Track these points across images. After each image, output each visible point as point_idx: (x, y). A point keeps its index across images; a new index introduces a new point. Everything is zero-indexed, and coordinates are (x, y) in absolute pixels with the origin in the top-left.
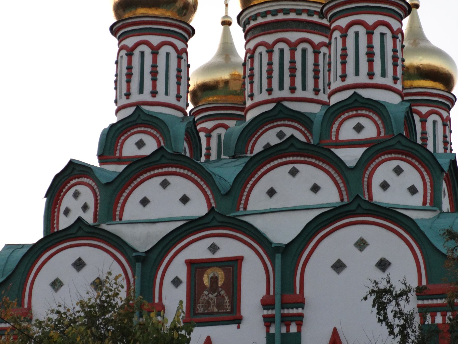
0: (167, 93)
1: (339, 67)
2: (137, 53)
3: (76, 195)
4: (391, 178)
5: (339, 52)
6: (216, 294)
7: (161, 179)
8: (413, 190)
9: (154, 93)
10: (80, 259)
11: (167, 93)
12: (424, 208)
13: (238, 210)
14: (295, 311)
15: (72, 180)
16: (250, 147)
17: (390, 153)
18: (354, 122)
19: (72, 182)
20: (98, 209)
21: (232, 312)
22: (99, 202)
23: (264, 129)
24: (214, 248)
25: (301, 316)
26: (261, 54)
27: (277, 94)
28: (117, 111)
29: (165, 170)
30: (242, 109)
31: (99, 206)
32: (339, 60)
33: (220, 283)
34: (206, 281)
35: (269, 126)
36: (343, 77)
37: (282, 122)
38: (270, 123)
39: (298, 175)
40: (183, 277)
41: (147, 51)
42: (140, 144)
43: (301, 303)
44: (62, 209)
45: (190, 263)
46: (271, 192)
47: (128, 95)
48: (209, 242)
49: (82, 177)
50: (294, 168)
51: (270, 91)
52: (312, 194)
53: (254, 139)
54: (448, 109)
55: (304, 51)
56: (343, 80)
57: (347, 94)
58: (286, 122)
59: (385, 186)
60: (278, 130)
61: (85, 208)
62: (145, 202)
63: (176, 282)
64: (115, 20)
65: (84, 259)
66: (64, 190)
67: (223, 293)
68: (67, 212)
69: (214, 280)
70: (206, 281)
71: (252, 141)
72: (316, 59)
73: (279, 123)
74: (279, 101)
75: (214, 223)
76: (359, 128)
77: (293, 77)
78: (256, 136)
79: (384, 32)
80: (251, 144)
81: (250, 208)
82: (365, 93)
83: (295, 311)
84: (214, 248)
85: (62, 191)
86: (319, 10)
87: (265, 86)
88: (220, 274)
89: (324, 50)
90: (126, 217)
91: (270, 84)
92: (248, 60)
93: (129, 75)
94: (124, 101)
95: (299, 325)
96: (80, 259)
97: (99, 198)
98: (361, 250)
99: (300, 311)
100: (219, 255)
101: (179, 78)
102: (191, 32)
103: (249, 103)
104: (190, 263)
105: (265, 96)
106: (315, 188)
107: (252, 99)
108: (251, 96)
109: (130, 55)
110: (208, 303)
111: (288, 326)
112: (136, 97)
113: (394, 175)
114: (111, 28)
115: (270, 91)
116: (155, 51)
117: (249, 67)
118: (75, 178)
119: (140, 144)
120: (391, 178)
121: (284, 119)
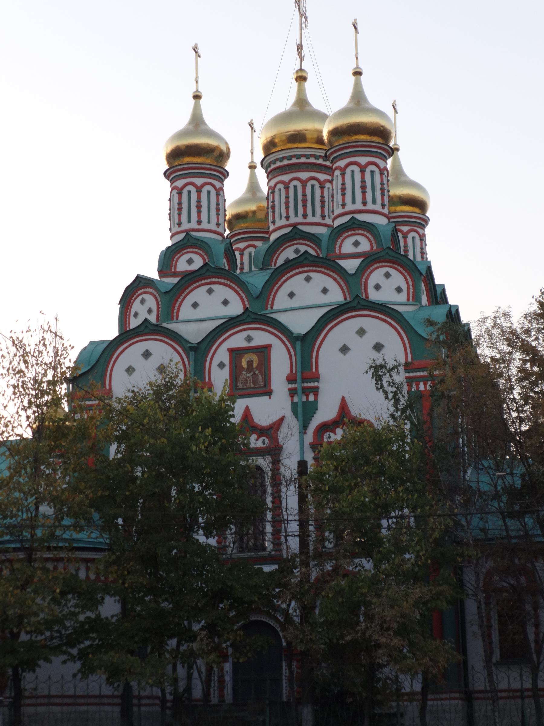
0: (209, 222)
2: (185, 192)
3: (143, 302)
4: (382, 281)
5: (340, 186)
8: (399, 290)
9: (199, 222)
10: (147, 350)
11: (209, 222)
12: (408, 303)
13: (267, 309)
15: (139, 290)
16: (274, 261)
19: (139, 292)
21: (264, 387)
23: (284, 247)
24: (249, 339)
25: (317, 388)
28: (172, 237)
29: (210, 280)
30: (267, 233)
32: (340, 192)
33: (255, 365)
34: (244, 364)
36: (344, 205)
37: (298, 241)
38: (289, 243)
39: (311, 281)
41: (357, 169)
42: (190, 261)
44: (132, 313)
45: (231, 351)
46: (291, 295)
47: (179, 224)
48: (245, 334)
49: (146, 288)
50: (308, 276)
51: (287, 218)
53: (277, 255)
54: (423, 227)
55: (313, 187)
56: (274, 225)
58: (301, 241)
61: (150, 311)
63: (221, 365)
64: (168, 167)
65: (151, 350)
66: (133, 299)
67: (257, 372)
68: (136, 315)
69: (250, 363)
70: (244, 364)
71: (275, 257)
72: (322, 193)
73: (295, 242)
75: (248, 320)
76: (356, 244)
77: (305, 206)
78: (278, 253)
79: (373, 170)
80: (274, 259)
81: (276, 307)
82: (361, 217)
84: (249, 339)
86: (324, 155)
87: (340, 202)
88: (255, 358)
89: (328, 185)
90: (181, 317)
91: (287, 212)
93: (180, 209)
95: (316, 395)
96: (147, 350)
97: (160, 303)
98: (361, 337)
99: (316, 384)
100: (253, 344)
101: (218, 210)
102: (226, 174)
104: (231, 351)
105: (284, 222)
106: (325, 291)
108: (274, 222)
109: (180, 193)
110: (246, 380)
111: (307, 396)
112: (185, 226)
113: (384, 279)
114: (165, 173)
116: (199, 190)
118: (141, 289)
119: (190, 261)
120: (382, 281)
121: (299, 239)
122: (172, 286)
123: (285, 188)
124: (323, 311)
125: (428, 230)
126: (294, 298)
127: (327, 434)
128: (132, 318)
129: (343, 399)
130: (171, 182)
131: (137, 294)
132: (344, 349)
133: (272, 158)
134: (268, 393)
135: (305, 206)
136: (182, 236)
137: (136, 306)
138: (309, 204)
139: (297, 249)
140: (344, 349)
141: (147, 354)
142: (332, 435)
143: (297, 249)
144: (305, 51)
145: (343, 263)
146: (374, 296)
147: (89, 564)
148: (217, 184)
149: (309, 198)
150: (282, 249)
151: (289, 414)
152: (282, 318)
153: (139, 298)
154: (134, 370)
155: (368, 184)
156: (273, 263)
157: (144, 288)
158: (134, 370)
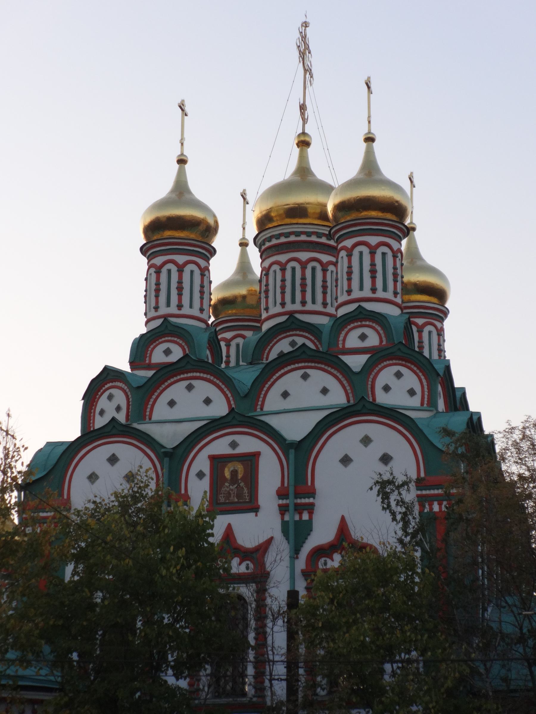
0: (191, 307)
1: (345, 283)
2: (164, 270)
4: (392, 382)
5: (345, 270)
6: (236, 485)
7: (186, 383)
8: (412, 392)
10: (114, 455)
14: (307, 501)
17: (392, 359)
18: (359, 331)
19: (106, 386)
20: (130, 410)
22: (130, 403)
23: (278, 338)
25: (312, 505)
26: (275, 272)
27: (289, 307)
29: (190, 375)
31: (130, 407)
33: (240, 476)
35: (283, 336)
36: (349, 292)
40: (207, 470)
42: (168, 352)
43: (312, 493)
44: (98, 410)
45: (213, 458)
47: (156, 308)
48: (230, 438)
49: (115, 382)
51: (283, 304)
52: (321, 395)
53: (269, 347)
55: (314, 269)
56: (267, 312)
57: (352, 307)
58: (298, 332)
59: (387, 388)
60: (290, 339)
62: (172, 403)
63: (200, 475)
65: (118, 455)
66: (99, 393)
67: (242, 484)
69: (234, 473)
73: (291, 333)
74: (291, 314)
76: (363, 337)
77: (304, 292)
81: (266, 408)
82: (369, 306)
83: (307, 501)
84: (234, 445)
85: (98, 394)
86: (327, 233)
87: (279, 300)
88: (240, 468)
89: (331, 268)
90: (155, 417)
91: (283, 298)
92: (264, 277)
93: (158, 291)
94: (153, 314)
95: (311, 513)
96: (114, 455)
98: (366, 446)
99: (311, 500)
100: (239, 451)
103: (264, 315)
104: (213, 458)
105: (278, 309)
106: (325, 391)
107: (267, 312)
108: (267, 309)
109: (158, 272)
111: (301, 514)
112: (163, 310)
113: (394, 379)
114: (141, 249)
115: (283, 304)
116: (181, 269)
117: (265, 284)
120: (392, 382)
122: (146, 380)
123: (281, 270)
124: (321, 415)
125: (447, 324)
126: (288, 399)
127: (322, 560)
128: (97, 416)
129: (343, 519)
130: (148, 258)
131: (104, 388)
132: (346, 460)
133: (267, 234)
134: (255, 509)
135: (304, 292)
136: (159, 322)
137: (103, 403)
138: (309, 289)
139: (293, 341)
140: (346, 460)
141: (113, 460)
142: (329, 561)
143: (293, 341)
144: (309, 112)
145: (347, 359)
146: (382, 398)
147: (36, 706)
148: (202, 263)
149: (309, 282)
150: (275, 340)
151: (278, 535)
152: (274, 421)
153: (107, 394)
154: (97, 477)
155: (379, 267)
156: (265, 356)
157: (112, 382)
158: (97, 477)
